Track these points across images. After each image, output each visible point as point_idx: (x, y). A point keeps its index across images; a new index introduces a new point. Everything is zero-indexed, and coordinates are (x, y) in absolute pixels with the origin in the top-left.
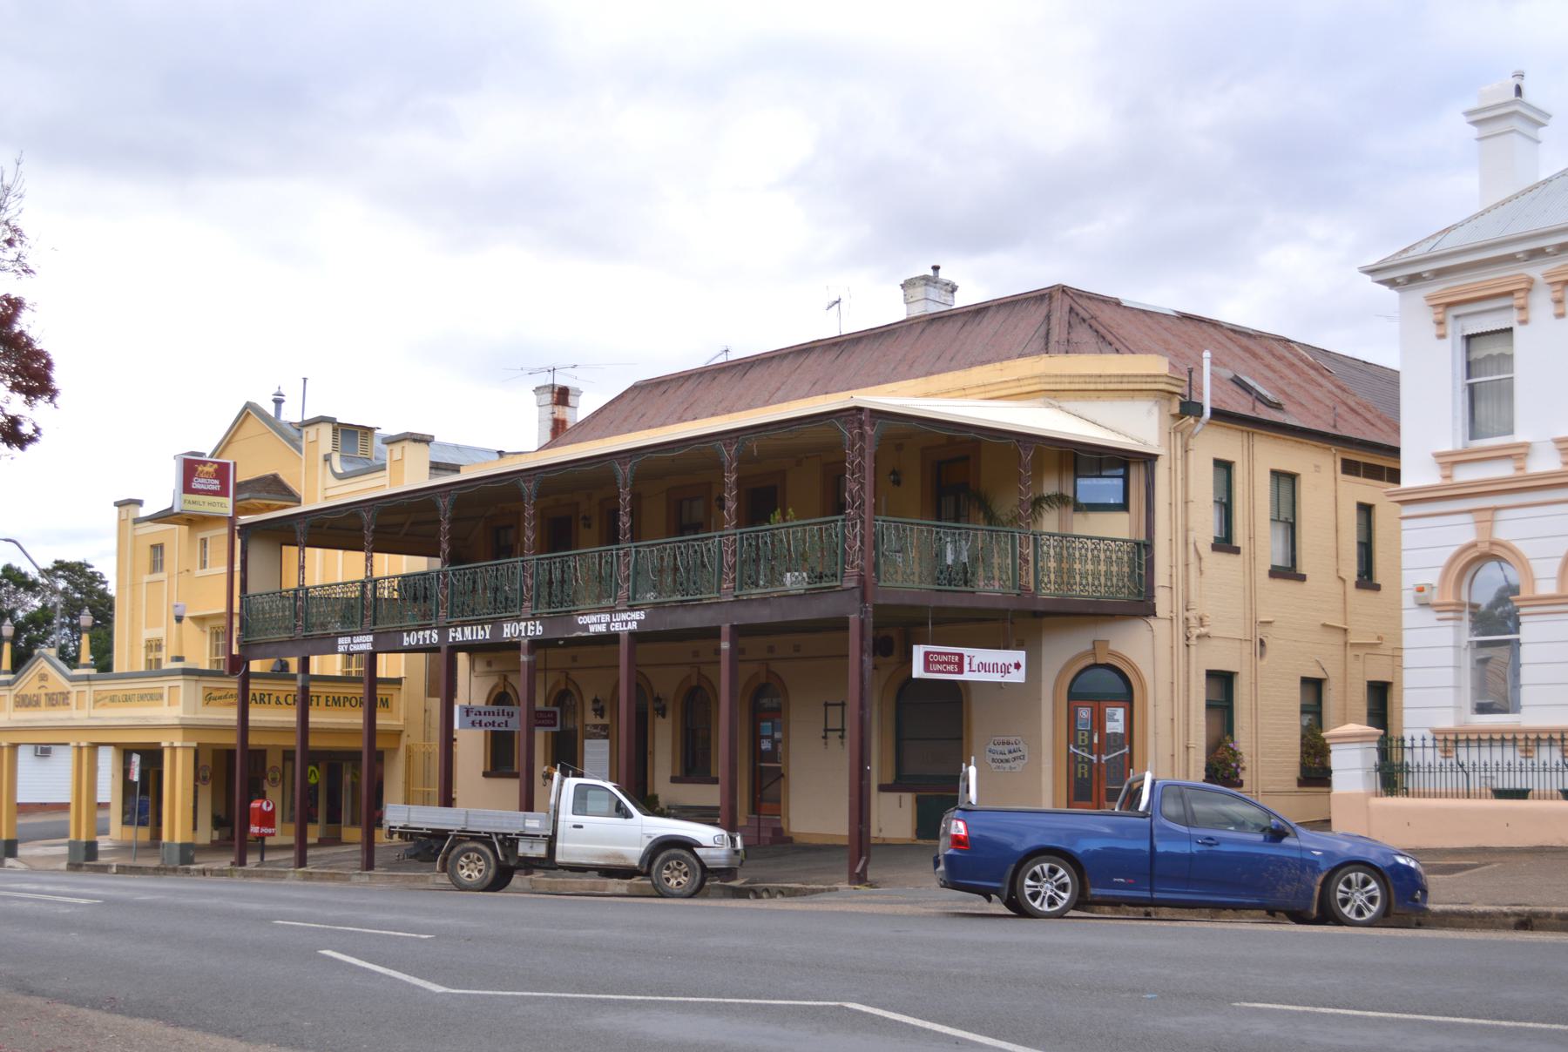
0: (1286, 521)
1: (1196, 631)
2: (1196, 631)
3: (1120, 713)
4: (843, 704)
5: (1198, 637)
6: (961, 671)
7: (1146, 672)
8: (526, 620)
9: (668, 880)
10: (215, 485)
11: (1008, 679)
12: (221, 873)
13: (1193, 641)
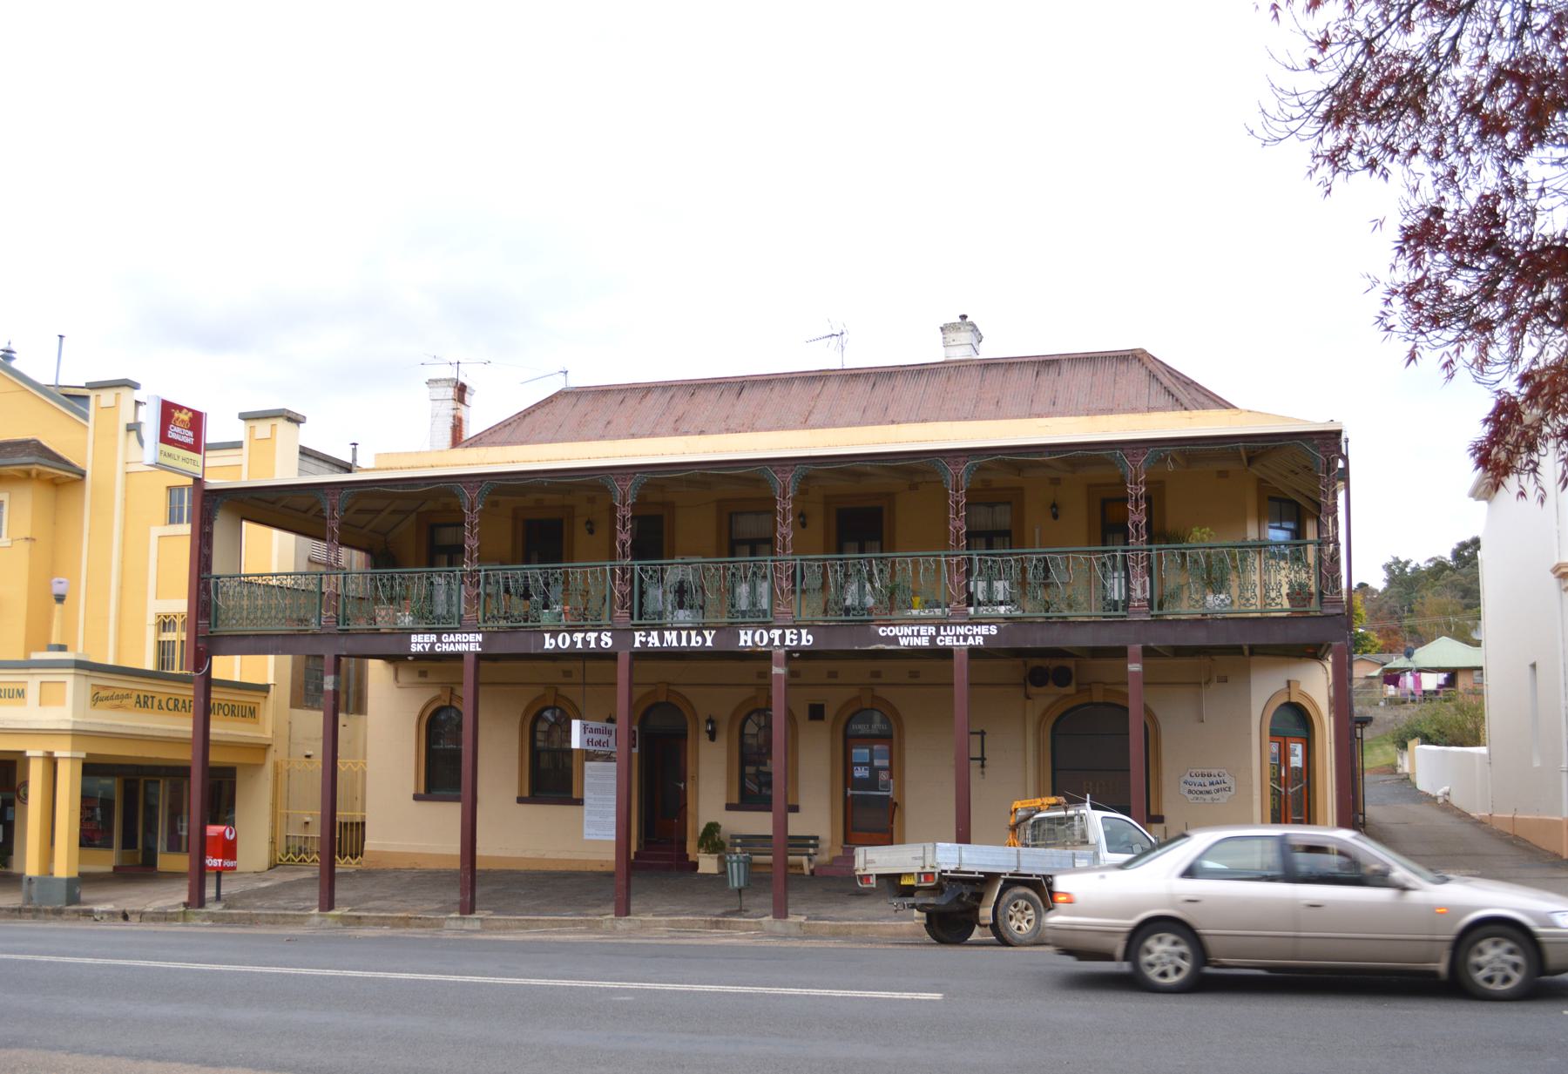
4: (983, 733)
8: (783, 627)
10: (188, 437)
12: (163, 916)
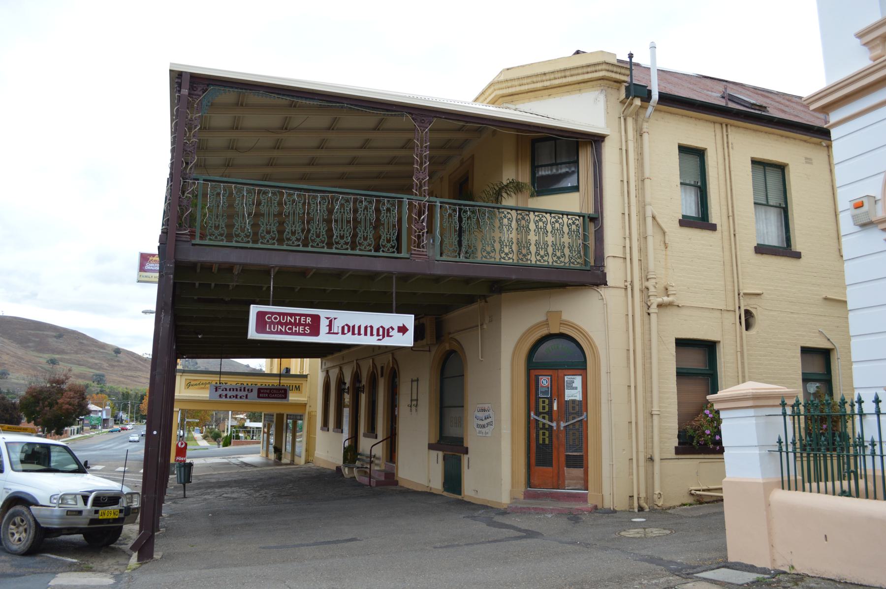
0: (779, 207)
1: (655, 301)
2: (655, 301)
3: (578, 381)
5: (660, 306)
6: (315, 331)
9: (13, 534)
11: (387, 342)
13: (654, 309)
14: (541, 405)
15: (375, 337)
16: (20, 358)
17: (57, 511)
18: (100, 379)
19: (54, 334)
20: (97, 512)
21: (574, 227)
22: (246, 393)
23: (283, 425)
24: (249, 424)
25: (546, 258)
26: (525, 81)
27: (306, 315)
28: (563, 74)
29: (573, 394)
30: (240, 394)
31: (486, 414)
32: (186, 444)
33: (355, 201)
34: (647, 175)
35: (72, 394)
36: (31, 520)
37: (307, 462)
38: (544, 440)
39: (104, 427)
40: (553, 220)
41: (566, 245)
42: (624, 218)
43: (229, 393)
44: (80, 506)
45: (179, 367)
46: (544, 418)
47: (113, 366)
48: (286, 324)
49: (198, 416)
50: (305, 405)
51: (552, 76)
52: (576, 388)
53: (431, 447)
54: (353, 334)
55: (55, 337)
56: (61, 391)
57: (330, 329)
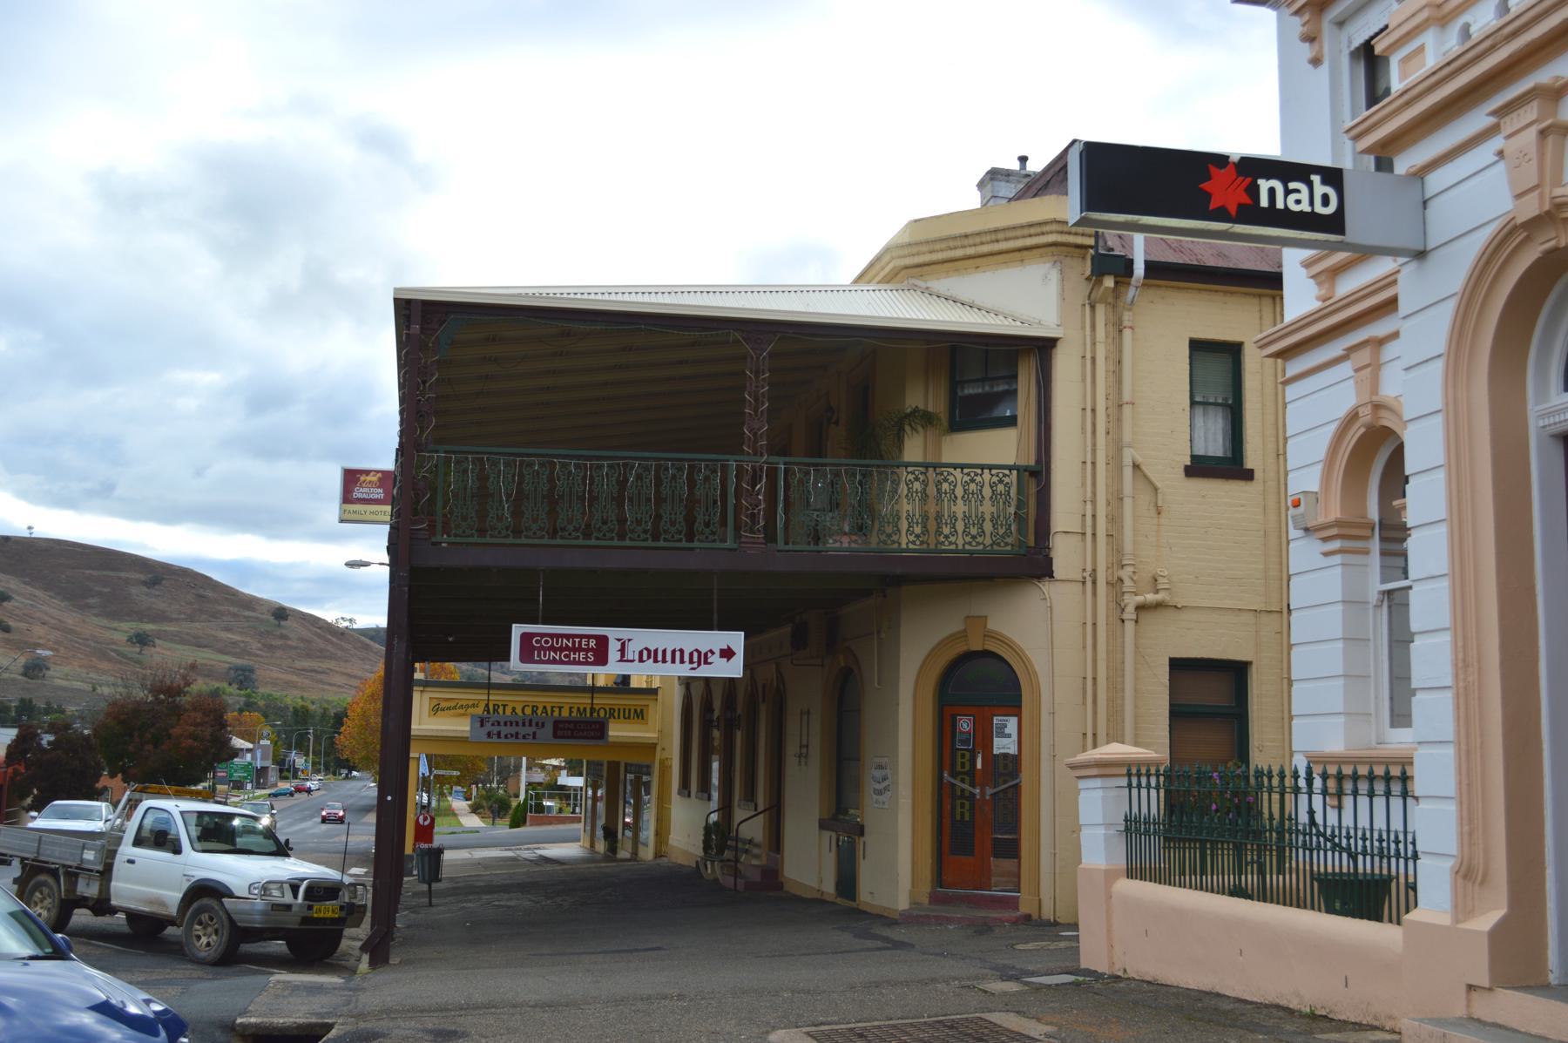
1: (1131, 601)
2: (1131, 601)
3: (1012, 723)
5: (1140, 608)
7: (1039, 661)
9: (199, 937)
11: (704, 672)
14: (959, 760)
15: (687, 665)
16: (71, 631)
17: (259, 904)
18: (243, 678)
19: (142, 577)
20: (310, 908)
21: (1001, 488)
22: (533, 729)
23: (622, 779)
24: (565, 780)
25: (952, 539)
26: (938, 246)
27: (589, 637)
28: (993, 237)
29: (1004, 745)
30: (522, 730)
31: (884, 772)
32: (433, 820)
33: (658, 468)
34: (1127, 397)
35: (198, 716)
36: (224, 917)
37: (658, 854)
38: (962, 814)
39: (259, 786)
40: (967, 478)
41: (988, 517)
42: (1084, 470)
43: (505, 730)
44: (288, 898)
45: (418, 676)
46: (963, 781)
47: (271, 648)
48: (561, 649)
49: (457, 767)
50: (653, 747)
51: (978, 240)
52: (1009, 736)
53: (823, 825)
54: (656, 661)
55: (145, 583)
56: (177, 711)
57: (623, 655)
